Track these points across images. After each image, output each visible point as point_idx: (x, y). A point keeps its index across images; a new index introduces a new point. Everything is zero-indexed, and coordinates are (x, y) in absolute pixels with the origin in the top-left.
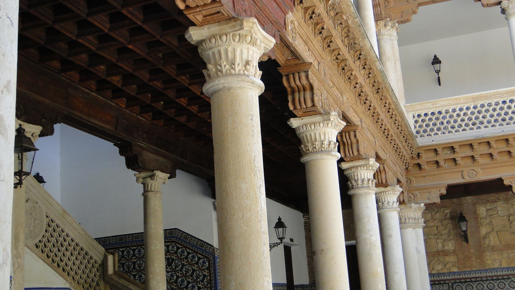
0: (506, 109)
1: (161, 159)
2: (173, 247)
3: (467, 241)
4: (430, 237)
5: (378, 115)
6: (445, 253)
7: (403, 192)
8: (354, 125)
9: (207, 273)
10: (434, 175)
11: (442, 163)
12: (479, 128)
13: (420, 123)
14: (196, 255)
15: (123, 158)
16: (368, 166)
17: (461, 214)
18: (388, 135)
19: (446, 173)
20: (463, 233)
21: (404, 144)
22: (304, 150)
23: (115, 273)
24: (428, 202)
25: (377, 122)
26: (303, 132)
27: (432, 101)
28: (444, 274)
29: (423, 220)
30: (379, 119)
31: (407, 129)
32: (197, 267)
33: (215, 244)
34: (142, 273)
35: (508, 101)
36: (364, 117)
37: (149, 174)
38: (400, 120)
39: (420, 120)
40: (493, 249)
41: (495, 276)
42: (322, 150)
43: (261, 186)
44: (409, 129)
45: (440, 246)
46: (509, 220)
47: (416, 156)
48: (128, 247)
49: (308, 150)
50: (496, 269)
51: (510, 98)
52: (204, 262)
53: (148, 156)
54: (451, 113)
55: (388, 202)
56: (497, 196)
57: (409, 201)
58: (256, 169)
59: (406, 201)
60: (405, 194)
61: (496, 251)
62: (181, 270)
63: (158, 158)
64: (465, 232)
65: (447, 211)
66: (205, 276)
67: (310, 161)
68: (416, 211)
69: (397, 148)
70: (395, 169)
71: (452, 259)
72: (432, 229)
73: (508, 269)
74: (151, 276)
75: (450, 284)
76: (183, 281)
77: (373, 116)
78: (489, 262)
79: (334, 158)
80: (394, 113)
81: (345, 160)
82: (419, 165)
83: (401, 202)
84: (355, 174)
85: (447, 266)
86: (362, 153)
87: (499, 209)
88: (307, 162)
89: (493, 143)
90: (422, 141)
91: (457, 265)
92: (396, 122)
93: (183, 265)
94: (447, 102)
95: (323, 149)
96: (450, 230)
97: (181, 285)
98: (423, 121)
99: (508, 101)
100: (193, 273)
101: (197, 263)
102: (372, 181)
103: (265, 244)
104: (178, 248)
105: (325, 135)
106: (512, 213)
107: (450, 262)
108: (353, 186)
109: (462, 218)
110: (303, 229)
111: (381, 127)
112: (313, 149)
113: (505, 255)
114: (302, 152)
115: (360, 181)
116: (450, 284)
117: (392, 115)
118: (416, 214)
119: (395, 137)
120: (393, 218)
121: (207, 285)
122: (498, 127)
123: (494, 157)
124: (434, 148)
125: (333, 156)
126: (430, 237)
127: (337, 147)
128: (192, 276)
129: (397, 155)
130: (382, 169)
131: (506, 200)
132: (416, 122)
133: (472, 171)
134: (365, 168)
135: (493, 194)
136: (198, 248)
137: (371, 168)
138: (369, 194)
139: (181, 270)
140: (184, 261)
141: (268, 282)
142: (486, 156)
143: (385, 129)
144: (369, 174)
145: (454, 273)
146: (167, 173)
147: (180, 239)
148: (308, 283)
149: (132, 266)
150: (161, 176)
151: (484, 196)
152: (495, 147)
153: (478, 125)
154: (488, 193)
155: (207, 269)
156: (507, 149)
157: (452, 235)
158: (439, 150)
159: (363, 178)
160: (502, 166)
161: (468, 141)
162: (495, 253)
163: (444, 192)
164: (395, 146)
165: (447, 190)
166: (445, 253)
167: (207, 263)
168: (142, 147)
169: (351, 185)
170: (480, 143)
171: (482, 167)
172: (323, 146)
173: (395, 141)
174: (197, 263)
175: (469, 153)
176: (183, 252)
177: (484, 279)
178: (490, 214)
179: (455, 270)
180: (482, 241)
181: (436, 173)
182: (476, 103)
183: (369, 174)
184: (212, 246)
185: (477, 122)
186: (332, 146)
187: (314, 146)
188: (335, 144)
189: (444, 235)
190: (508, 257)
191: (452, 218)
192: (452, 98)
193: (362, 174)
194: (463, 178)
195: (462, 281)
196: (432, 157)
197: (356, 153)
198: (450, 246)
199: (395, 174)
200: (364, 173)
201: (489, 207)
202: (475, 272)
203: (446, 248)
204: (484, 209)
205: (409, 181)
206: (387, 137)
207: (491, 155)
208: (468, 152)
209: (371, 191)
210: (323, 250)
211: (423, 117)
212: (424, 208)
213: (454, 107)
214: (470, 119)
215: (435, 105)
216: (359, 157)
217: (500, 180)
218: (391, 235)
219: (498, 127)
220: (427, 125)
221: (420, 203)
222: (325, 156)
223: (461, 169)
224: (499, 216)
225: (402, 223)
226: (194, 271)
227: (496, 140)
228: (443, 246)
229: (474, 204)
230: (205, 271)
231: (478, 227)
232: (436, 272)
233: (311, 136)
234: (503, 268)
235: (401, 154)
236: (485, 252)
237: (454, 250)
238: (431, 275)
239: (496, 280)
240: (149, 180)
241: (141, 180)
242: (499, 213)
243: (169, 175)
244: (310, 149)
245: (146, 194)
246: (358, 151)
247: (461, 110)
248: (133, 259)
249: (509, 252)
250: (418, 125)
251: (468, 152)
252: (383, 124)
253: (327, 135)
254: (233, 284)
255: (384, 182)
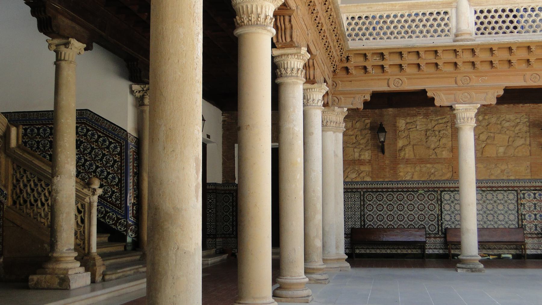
0: (439, 21)
1: (77, 27)
2: (82, 129)
3: (383, 152)
4: (348, 145)
5: (314, 5)
6: (361, 162)
7: (327, 93)
8: (290, 9)
9: (119, 158)
10: (360, 81)
11: (369, 69)
12: (410, 37)
13: (353, 26)
14: (108, 139)
15: (34, 20)
16: (299, 55)
17: (381, 125)
18: (321, 30)
19: (372, 79)
20: (380, 144)
21: (335, 43)
22: (239, 22)
23: (18, 146)
24: (351, 107)
25: (312, 13)
26: (239, 3)
27: (368, 4)
28: (357, 183)
29: (344, 125)
30: (314, 10)
31: (341, 28)
32: (107, 152)
33: (130, 127)
34: (46, 154)
35: (442, 13)
36: (300, 3)
37: (64, 41)
38: (335, 16)
39: (354, 22)
40: (407, 162)
41: (405, 188)
42: (257, 24)
43: (199, 33)
44: (342, 29)
45: (357, 155)
46: (426, 134)
47: (345, 59)
48: (32, 125)
49: (243, 22)
50: (408, 182)
51: (444, 10)
52: (115, 147)
53: (63, 22)
54: (385, 19)
55: (313, 100)
56: (417, 110)
57: (332, 104)
58: (195, 15)
59: (330, 103)
60: (330, 96)
61: (410, 164)
62: (90, 153)
63: (74, 25)
64: (383, 142)
65: (368, 121)
66: (115, 161)
67: (244, 34)
68: (338, 115)
69: (328, 47)
70: (323, 69)
71: (366, 168)
72: (351, 137)
73: (418, 182)
74: (60, 150)
75: (362, 193)
76: (91, 165)
77: (309, 5)
78: (401, 174)
79: (269, 33)
80: (330, 7)
81: (277, 46)
82: (347, 69)
83: (326, 105)
84: (285, 62)
85: (361, 175)
86: (294, 40)
87: (418, 123)
88: (240, 35)
89: (422, 54)
90: (353, 45)
91: (370, 175)
92: (331, 17)
93: (93, 149)
94: (382, 7)
95: (259, 23)
96: (368, 140)
97: (89, 169)
98: (357, 24)
99: (442, 13)
100: (102, 158)
101: (108, 148)
102: (302, 71)
103: (198, 93)
104: (88, 130)
105: (262, 8)
106: (430, 128)
107: (364, 171)
108: (281, 74)
109: (382, 129)
110: (221, 127)
111: (315, 20)
112: (248, 21)
113: (418, 168)
114: (236, 24)
115: (289, 70)
116: (362, 193)
117: (328, 8)
118: (338, 119)
119: (327, 34)
120: (317, 115)
121: (118, 170)
122: (429, 38)
123: (421, 67)
124: (364, 52)
125: (268, 31)
126: (348, 145)
127: (273, 23)
128: (101, 160)
129: (327, 54)
130: (311, 63)
131: (426, 115)
132: (349, 24)
133: (397, 80)
134: (296, 57)
135: (415, 108)
136: (110, 132)
137: (302, 57)
138: (296, 84)
139: (90, 153)
140: (93, 144)
141: (198, 131)
142: (414, 66)
143: (319, 23)
144: (299, 63)
145: (367, 182)
146: (83, 43)
147: (90, 121)
148: (221, 182)
149: (35, 146)
150: (77, 45)
151: (406, 110)
152: (424, 58)
153: (410, 34)
154: (409, 106)
155: (118, 154)
156: (435, 61)
157: (370, 145)
158: (369, 56)
159: (292, 66)
160: (428, 78)
161: (398, 48)
162: (408, 165)
163: (368, 98)
164: (327, 44)
165: (371, 97)
166: (361, 162)
167: (119, 149)
168: (56, 9)
169: (279, 73)
170: (409, 52)
171: (409, 77)
172: (259, 19)
173: (327, 38)
174: (108, 148)
175: (397, 61)
176: (93, 135)
177: (395, 190)
178: (409, 128)
179: (368, 179)
180: (398, 154)
181: (364, 78)
182: (411, 12)
183: (299, 63)
184: (126, 131)
185: (410, 31)
186: (268, 20)
187: (250, 18)
188: (271, 19)
189: (362, 144)
190: (420, 171)
191: (372, 128)
192: (388, 3)
193: (292, 62)
194: (389, 86)
195: (374, 190)
196: (360, 61)
197: (288, 39)
198: (366, 155)
199: (323, 72)
200: (295, 62)
201: (408, 121)
202: (387, 183)
203: (362, 157)
204: (404, 122)
205: (335, 84)
206: (320, 32)
207: (419, 65)
208: (397, 60)
209: (299, 81)
210: (249, 125)
211: (356, 20)
212: (347, 113)
213: (389, 13)
214: (403, 27)
215: (370, 9)
216: (291, 45)
217: (424, 92)
218: (313, 133)
219: (429, 38)
220: (360, 29)
221: (343, 107)
222: (260, 31)
223: (387, 77)
224: (417, 130)
225: (325, 125)
226: (104, 155)
227: (426, 51)
228: (360, 155)
229: (395, 116)
230: (116, 157)
231: (395, 139)
232: (350, 180)
233: (247, 7)
234: (415, 181)
235: (331, 54)
236: (399, 164)
237: (369, 160)
238: (345, 183)
239: (406, 191)
240: (62, 48)
241: (54, 47)
242: (418, 128)
243: (85, 46)
244: (245, 22)
245: (58, 63)
246: (291, 37)
247: (395, 16)
248: (37, 138)
249: (422, 166)
250: (350, 28)
251: (397, 60)
252: (318, 16)
253: (264, 9)
254: (163, 128)
255: (312, 78)
